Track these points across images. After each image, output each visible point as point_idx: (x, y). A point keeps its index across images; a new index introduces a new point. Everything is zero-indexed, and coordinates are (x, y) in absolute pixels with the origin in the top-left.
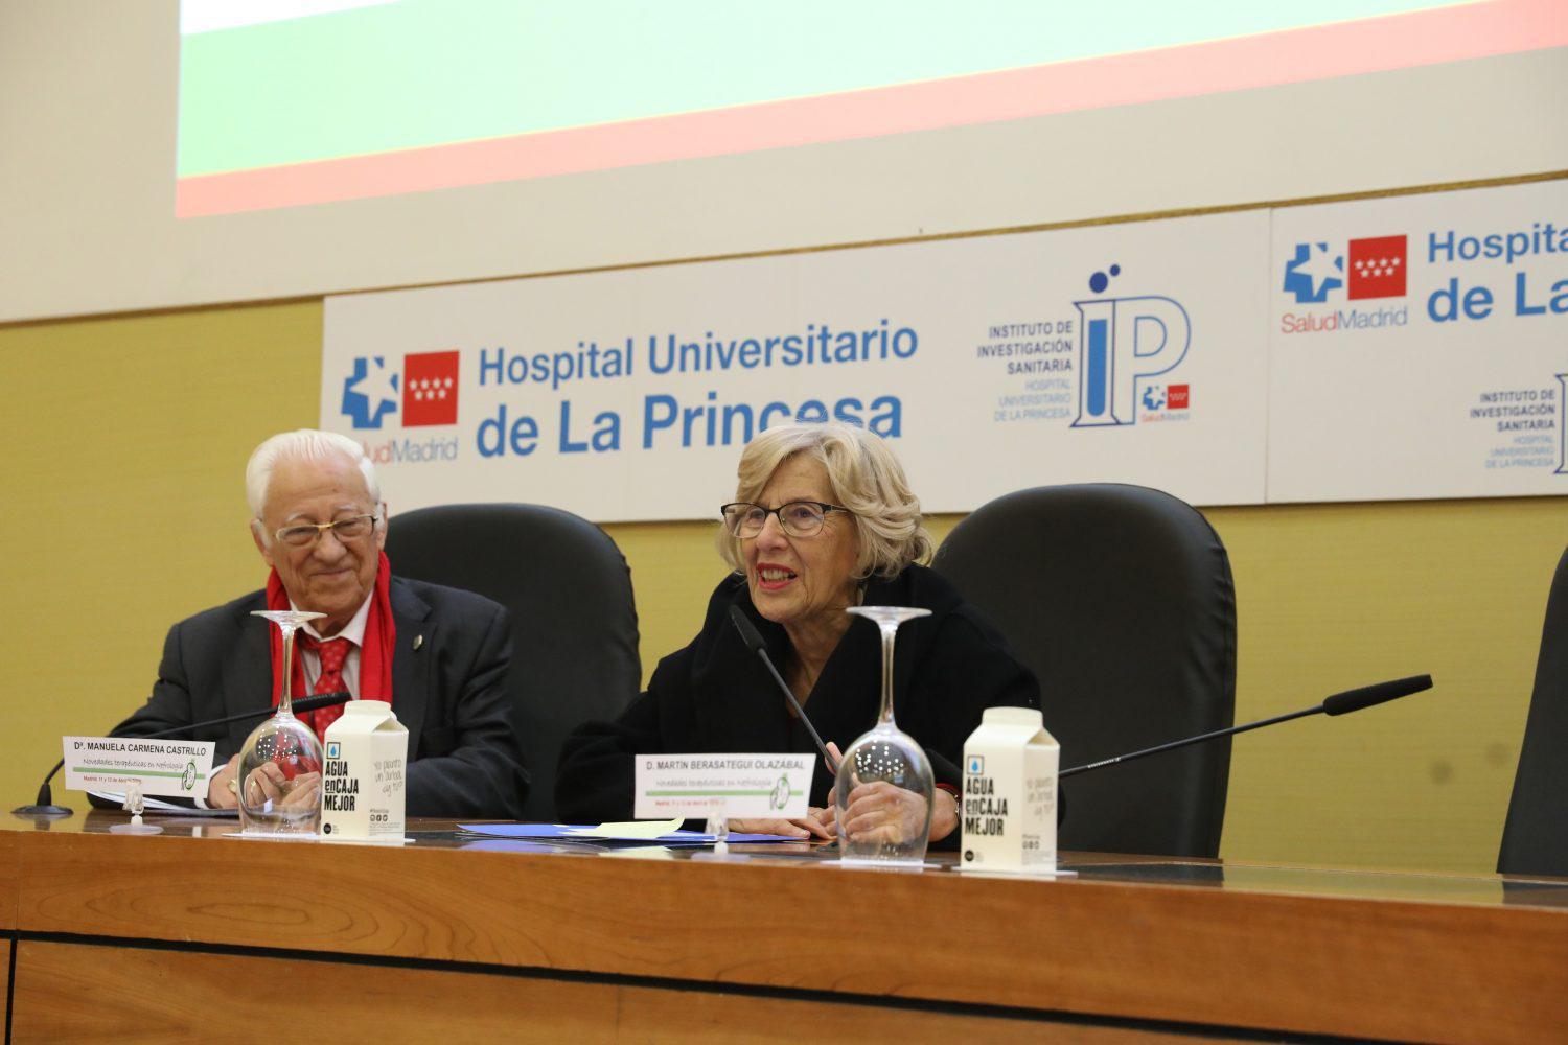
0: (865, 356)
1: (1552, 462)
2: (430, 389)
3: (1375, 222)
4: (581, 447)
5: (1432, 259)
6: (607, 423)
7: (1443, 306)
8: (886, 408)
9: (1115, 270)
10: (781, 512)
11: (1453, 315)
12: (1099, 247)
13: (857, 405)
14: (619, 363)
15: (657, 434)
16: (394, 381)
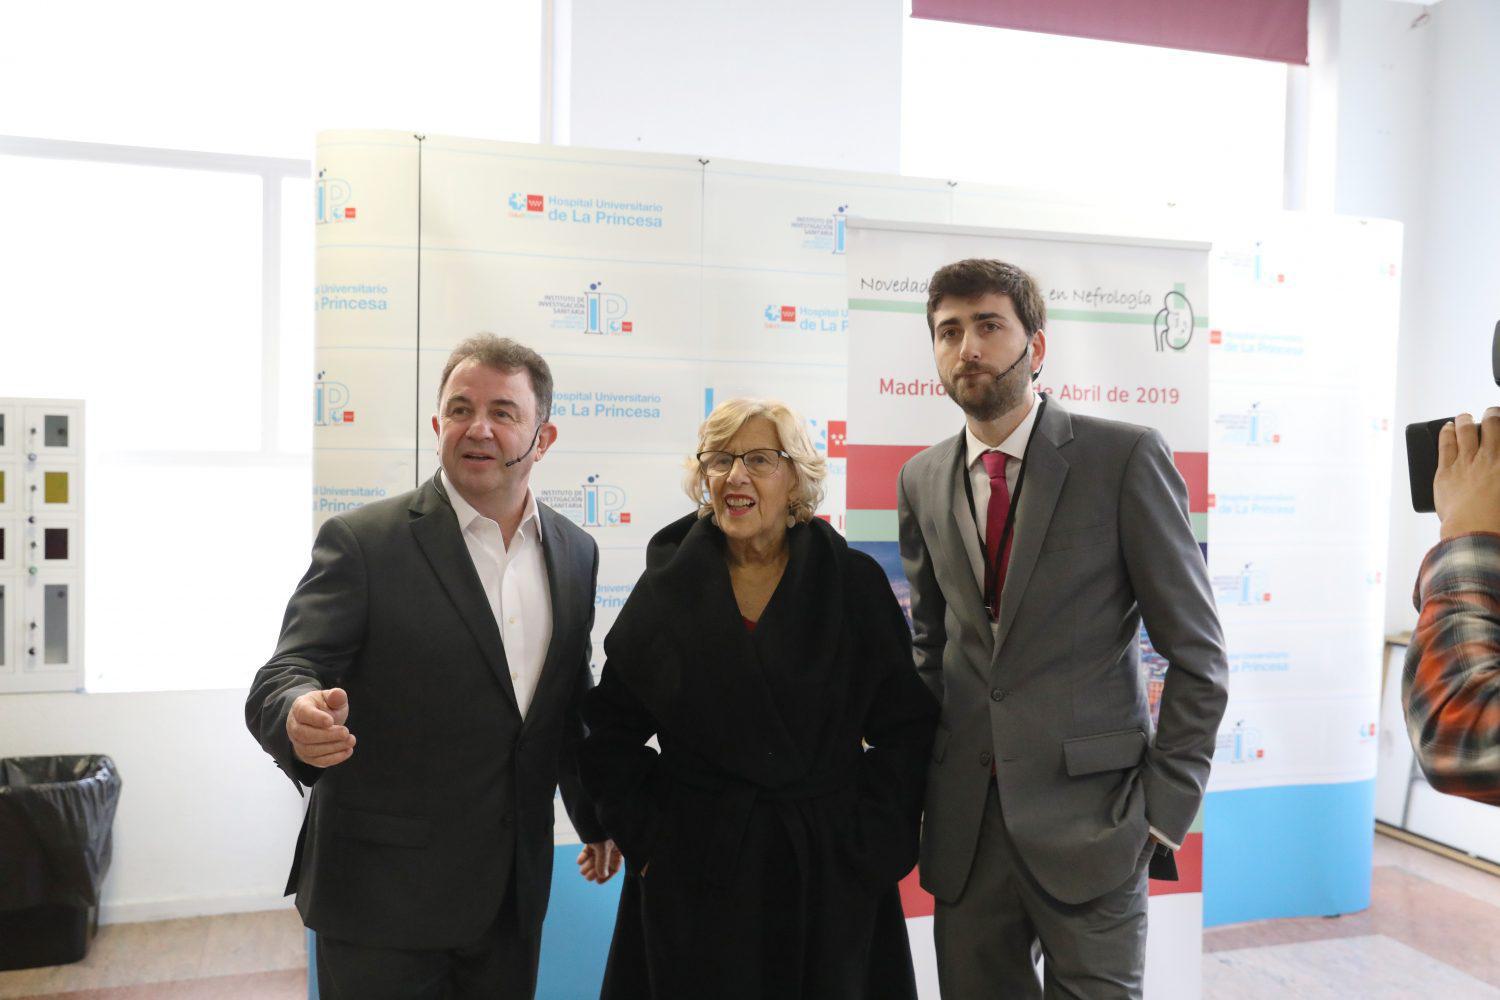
7: (803, 325)
10: (746, 457)
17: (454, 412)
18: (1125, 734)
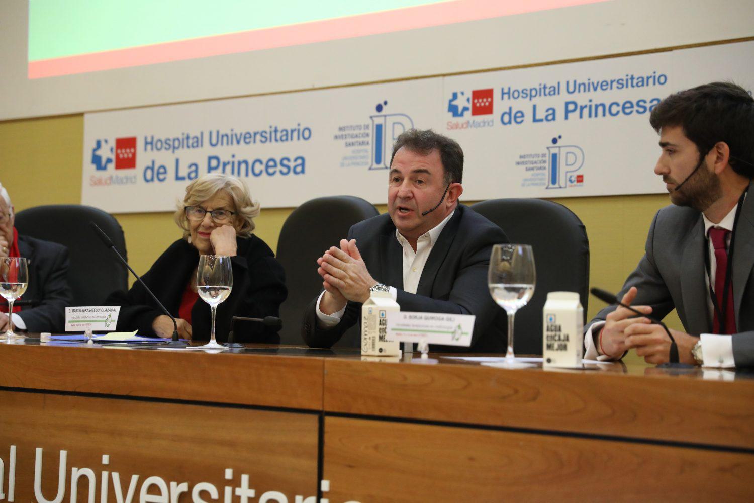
0: (292, 139)
1: (545, 184)
2: (126, 154)
3: (482, 83)
4: (541, 120)
5: (502, 98)
6: (551, 112)
7: (506, 118)
8: (299, 162)
9: (385, 103)
11: (510, 122)
12: (378, 94)
13: (288, 160)
14: (555, 90)
15: (570, 115)
16: (112, 150)
17: (394, 180)
18: (93, 317)
